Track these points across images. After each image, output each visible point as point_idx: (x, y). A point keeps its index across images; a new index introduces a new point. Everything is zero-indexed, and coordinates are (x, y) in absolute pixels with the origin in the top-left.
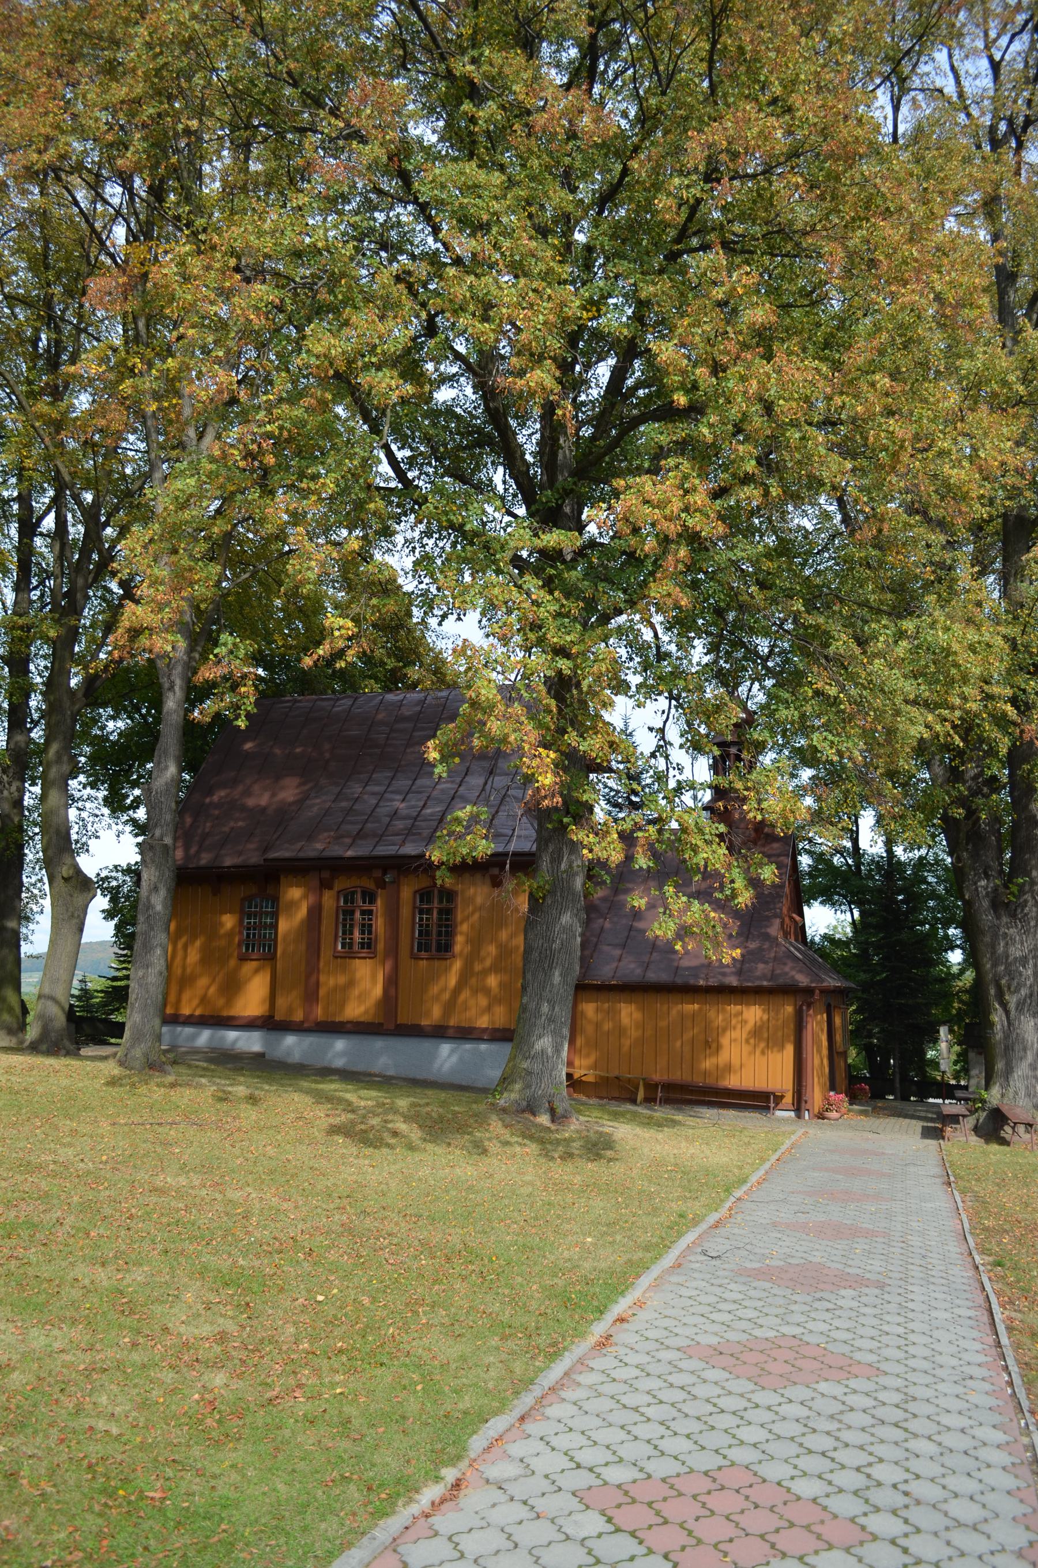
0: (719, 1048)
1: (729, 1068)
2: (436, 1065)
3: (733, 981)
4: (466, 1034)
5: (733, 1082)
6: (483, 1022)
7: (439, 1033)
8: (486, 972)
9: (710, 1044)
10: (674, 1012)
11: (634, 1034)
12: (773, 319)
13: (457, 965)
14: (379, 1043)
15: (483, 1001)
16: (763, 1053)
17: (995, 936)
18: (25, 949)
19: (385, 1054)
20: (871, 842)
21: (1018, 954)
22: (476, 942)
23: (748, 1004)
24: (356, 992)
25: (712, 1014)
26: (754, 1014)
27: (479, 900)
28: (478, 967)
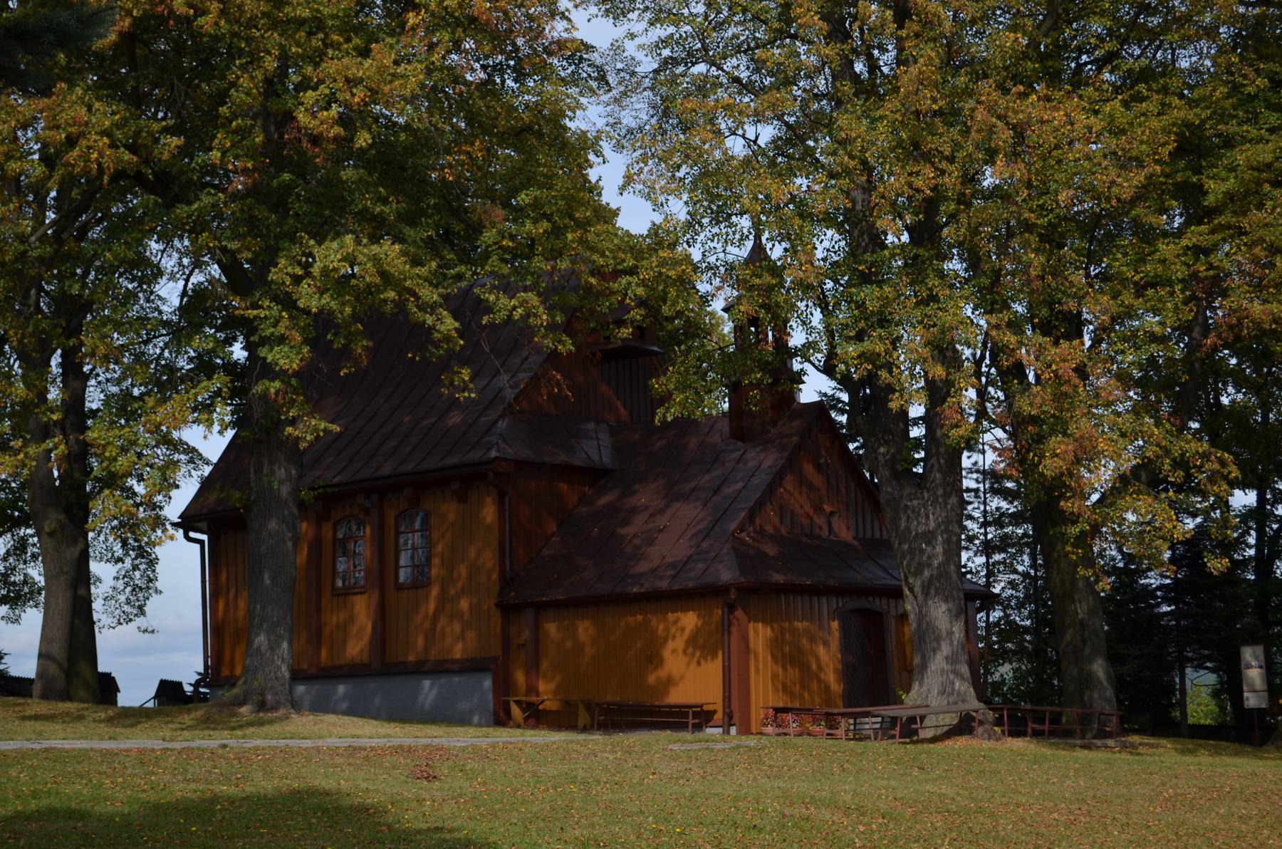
1: (669, 683)
2: (421, 699)
3: (663, 584)
4: (440, 669)
5: (676, 697)
6: (458, 652)
7: (420, 669)
9: (653, 658)
11: (589, 651)
13: (435, 591)
14: (372, 685)
15: (457, 627)
16: (699, 664)
21: (921, 529)
23: (685, 610)
24: (355, 629)
25: (654, 622)
26: (690, 620)
27: (451, 517)
28: (452, 592)
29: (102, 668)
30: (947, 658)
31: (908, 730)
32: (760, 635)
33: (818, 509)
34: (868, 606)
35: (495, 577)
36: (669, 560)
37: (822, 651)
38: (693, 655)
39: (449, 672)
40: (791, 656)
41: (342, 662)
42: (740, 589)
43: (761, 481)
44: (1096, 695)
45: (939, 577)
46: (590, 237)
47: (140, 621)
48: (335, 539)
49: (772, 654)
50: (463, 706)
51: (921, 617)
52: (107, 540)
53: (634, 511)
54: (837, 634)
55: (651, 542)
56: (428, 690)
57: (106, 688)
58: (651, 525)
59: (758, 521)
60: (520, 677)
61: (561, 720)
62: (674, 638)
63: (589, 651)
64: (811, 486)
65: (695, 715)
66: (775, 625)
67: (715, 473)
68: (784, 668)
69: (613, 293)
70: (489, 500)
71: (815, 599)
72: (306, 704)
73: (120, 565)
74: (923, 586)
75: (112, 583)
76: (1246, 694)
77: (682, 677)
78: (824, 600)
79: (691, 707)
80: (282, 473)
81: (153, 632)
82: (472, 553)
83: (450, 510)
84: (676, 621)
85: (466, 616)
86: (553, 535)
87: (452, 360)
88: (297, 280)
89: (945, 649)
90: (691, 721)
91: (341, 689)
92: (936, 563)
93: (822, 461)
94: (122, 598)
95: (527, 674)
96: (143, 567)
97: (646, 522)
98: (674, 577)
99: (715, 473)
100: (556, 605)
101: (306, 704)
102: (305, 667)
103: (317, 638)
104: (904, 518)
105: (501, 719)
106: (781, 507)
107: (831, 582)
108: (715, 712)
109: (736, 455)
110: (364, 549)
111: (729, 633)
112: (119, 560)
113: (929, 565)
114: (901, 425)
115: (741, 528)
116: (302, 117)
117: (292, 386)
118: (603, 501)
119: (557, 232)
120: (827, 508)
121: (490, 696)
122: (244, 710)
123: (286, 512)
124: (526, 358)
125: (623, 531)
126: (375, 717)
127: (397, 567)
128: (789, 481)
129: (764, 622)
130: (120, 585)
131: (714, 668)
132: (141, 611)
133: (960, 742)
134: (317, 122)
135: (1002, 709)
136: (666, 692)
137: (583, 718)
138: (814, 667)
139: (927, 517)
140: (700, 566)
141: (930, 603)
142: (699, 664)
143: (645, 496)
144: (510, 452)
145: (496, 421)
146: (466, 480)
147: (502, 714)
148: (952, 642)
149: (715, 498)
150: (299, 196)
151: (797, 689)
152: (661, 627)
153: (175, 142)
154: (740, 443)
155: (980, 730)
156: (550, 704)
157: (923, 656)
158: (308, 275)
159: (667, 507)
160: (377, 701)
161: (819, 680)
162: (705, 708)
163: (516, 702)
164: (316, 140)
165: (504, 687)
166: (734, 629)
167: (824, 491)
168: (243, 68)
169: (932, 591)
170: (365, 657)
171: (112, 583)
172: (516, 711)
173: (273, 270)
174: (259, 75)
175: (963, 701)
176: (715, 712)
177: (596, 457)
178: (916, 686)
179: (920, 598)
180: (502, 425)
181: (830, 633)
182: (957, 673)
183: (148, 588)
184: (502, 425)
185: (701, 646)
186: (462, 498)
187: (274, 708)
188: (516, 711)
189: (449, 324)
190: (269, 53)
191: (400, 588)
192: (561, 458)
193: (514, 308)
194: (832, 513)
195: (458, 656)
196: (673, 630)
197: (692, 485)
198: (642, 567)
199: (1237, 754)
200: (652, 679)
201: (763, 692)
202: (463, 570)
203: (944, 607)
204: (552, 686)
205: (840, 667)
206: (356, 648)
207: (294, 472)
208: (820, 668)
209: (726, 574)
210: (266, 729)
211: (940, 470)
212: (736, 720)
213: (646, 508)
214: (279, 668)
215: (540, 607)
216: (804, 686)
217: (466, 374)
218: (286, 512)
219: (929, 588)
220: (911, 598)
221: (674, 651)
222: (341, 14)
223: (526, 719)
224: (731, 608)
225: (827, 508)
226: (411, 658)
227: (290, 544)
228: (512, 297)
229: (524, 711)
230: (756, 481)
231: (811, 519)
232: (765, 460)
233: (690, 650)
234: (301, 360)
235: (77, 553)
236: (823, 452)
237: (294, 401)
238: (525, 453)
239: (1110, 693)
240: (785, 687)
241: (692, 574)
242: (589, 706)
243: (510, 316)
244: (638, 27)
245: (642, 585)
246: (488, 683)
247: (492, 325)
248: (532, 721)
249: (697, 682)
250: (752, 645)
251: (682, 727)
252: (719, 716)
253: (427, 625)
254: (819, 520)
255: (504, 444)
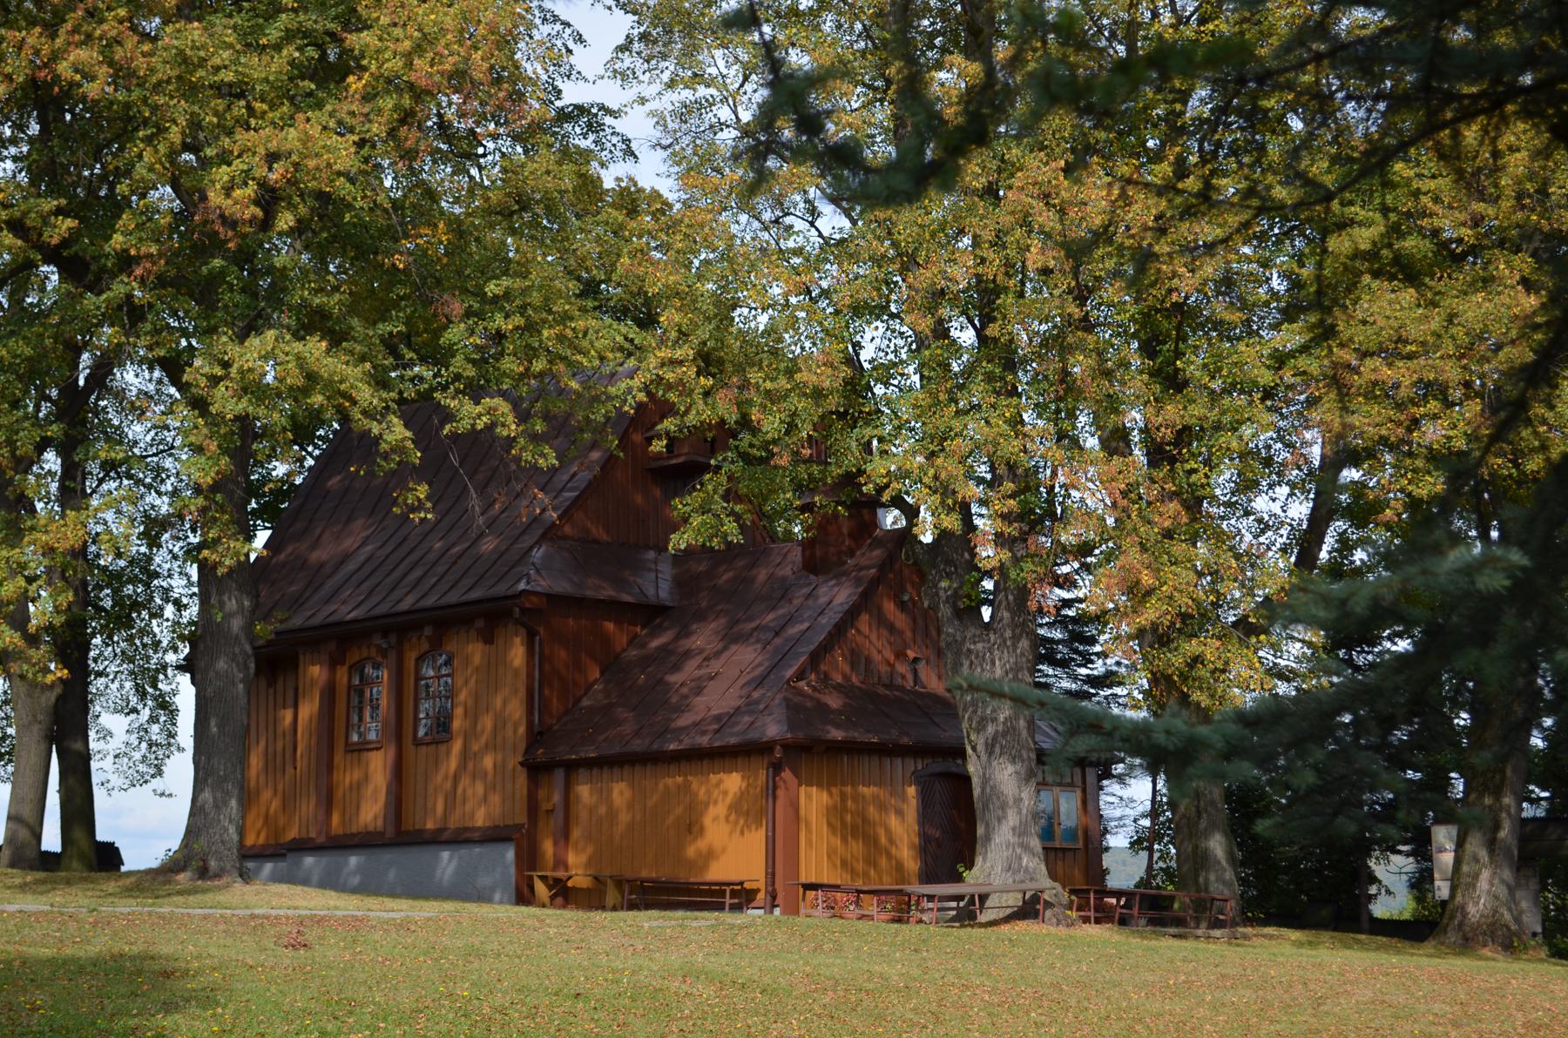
0: (702, 830)
1: (710, 855)
2: (439, 873)
3: (704, 741)
4: (460, 838)
5: (718, 872)
6: (480, 819)
7: (437, 839)
8: (477, 756)
9: (692, 826)
10: (661, 786)
11: (624, 817)
12: (75, 864)
14: (387, 856)
15: (480, 788)
16: (742, 833)
17: (958, 654)
18: (1530, 357)
19: (393, 863)
20: (571, 622)
22: (473, 715)
25: (695, 785)
26: (733, 782)
27: (477, 660)
28: (475, 747)
29: (102, 835)
30: (1014, 829)
31: (967, 913)
32: (814, 801)
33: (901, 655)
34: (954, 769)
35: (522, 730)
36: (715, 712)
37: (893, 821)
38: (736, 823)
39: (468, 841)
40: (855, 827)
41: (354, 830)
42: (787, 747)
43: (828, 621)
44: (1212, 877)
45: (1005, 734)
46: (569, 333)
47: (156, 783)
48: (350, 687)
49: (829, 824)
50: (484, 880)
51: (985, 780)
52: (122, 687)
53: (687, 654)
54: (914, 802)
55: (699, 691)
56: (447, 862)
57: (108, 857)
58: (703, 672)
59: (823, 667)
60: (548, 847)
61: (591, 899)
62: (716, 802)
63: (624, 817)
64: (891, 628)
65: (734, 894)
66: (834, 790)
67: (781, 612)
68: (844, 840)
69: (610, 398)
70: (518, 640)
71: (887, 761)
72: (315, 878)
73: (133, 716)
74: (986, 744)
75: (125, 737)
76: (1437, 883)
77: (724, 849)
78: (898, 761)
79: (728, 884)
80: (232, 605)
81: (170, 795)
82: (498, 702)
83: (476, 652)
84: (720, 782)
85: (490, 777)
86: (596, 681)
87: (404, 474)
88: (215, 380)
89: (1012, 819)
90: (728, 901)
91: (353, 860)
92: (1002, 718)
93: (906, 598)
94: (137, 756)
95: (556, 843)
96: (163, 719)
97: (699, 667)
98: (717, 731)
99: (781, 612)
100: (589, 764)
101: (315, 878)
102: (313, 835)
103: (328, 801)
104: (966, 663)
105: (524, 896)
106: (853, 651)
107: (905, 740)
108: (758, 890)
109: (806, 591)
110: (382, 692)
111: (775, 798)
112: (135, 711)
113: (994, 720)
114: (967, 555)
115: (800, 675)
116: (215, 198)
117: (216, 503)
118: (655, 643)
119: (531, 328)
120: (911, 654)
121: (513, 870)
122: (181, 877)
123: (237, 650)
124: (574, 475)
125: (674, 678)
126: (393, 895)
127: (416, 720)
128: (864, 622)
129: (819, 785)
130: (133, 739)
131: (757, 839)
132: (159, 772)
133: (1021, 926)
134: (229, 202)
135: (1088, 891)
136: (705, 867)
137: (612, 896)
138: (883, 840)
139: (993, 663)
140: (747, 719)
141: (995, 763)
142: (742, 833)
143: (703, 638)
144: (543, 584)
145: (531, 549)
146: (491, 617)
147: (526, 890)
148: (1020, 813)
149: (777, 641)
150: (231, 286)
151: (860, 867)
152: (703, 791)
153: (70, 223)
154: (812, 577)
155: (1048, 913)
156: (580, 879)
157: (987, 825)
158: (227, 376)
159: (725, 648)
160: (392, 874)
161: (889, 856)
162: (746, 885)
163: (541, 877)
164: (230, 222)
165: (529, 859)
166: (780, 793)
167: (909, 634)
168: (149, 140)
169: (997, 750)
170: (380, 823)
171: (125, 737)
172: (541, 889)
173: (188, 370)
174: (162, 148)
175: (1032, 879)
176: (758, 890)
177: (651, 591)
178: (979, 860)
179: (984, 758)
180: (538, 554)
181: (904, 798)
182: (1026, 848)
183: (169, 744)
184: (538, 554)
185: (746, 812)
186: (488, 639)
187: (218, 876)
188: (541, 889)
189: (397, 432)
190: (174, 122)
191: (418, 743)
192: (608, 592)
193: (479, 416)
194: (916, 660)
195: (479, 823)
196: (716, 793)
197: (754, 625)
198: (684, 721)
199: (1398, 952)
200: (691, 852)
201: (815, 863)
202: (487, 722)
203: (1010, 769)
204: (583, 858)
205: (917, 840)
206: (371, 812)
207: (246, 603)
208: (891, 841)
209: (773, 729)
210: (199, 897)
211: (1008, 608)
212: (779, 900)
213: (701, 651)
214: (226, 830)
215: (571, 767)
216: (871, 862)
217: (422, 491)
218: (237, 650)
219: (993, 746)
220: (974, 757)
221: (715, 819)
222: (271, 78)
223: (552, 898)
224: (777, 768)
225: (911, 654)
226: (430, 825)
227: (241, 686)
228: (477, 403)
229: (550, 888)
230: (823, 620)
231: (892, 666)
232: (840, 595)
233: (733, 817)
234: (218, 473)
235: (53, 699)
236: (909, 587)
237: (215, 519)
238: (562, 586)
239: (1229, 875)
240: (844, 863)
241: (737, 729)
242: (619, 883)
243: (473, 425)
244: (650, 91)
245: (681, 741)
246: (510, 854)
247: (454, 436)
248: (559, 900)
249: (736, 854)
250: (802, 812)
251: (720, 907)
252: (761, 896)
253: (449, 785)
254: (901, 668)
255: (542, 575)
